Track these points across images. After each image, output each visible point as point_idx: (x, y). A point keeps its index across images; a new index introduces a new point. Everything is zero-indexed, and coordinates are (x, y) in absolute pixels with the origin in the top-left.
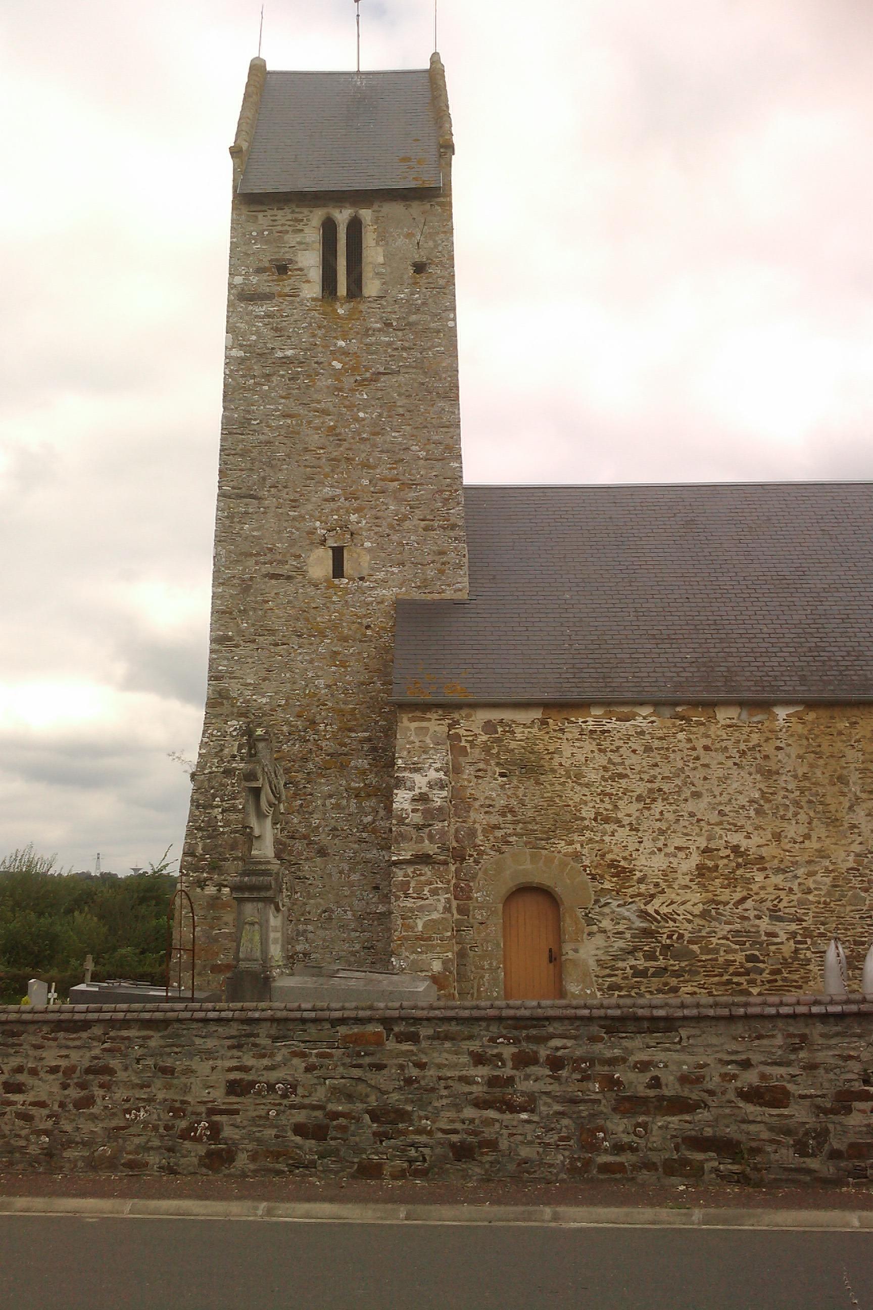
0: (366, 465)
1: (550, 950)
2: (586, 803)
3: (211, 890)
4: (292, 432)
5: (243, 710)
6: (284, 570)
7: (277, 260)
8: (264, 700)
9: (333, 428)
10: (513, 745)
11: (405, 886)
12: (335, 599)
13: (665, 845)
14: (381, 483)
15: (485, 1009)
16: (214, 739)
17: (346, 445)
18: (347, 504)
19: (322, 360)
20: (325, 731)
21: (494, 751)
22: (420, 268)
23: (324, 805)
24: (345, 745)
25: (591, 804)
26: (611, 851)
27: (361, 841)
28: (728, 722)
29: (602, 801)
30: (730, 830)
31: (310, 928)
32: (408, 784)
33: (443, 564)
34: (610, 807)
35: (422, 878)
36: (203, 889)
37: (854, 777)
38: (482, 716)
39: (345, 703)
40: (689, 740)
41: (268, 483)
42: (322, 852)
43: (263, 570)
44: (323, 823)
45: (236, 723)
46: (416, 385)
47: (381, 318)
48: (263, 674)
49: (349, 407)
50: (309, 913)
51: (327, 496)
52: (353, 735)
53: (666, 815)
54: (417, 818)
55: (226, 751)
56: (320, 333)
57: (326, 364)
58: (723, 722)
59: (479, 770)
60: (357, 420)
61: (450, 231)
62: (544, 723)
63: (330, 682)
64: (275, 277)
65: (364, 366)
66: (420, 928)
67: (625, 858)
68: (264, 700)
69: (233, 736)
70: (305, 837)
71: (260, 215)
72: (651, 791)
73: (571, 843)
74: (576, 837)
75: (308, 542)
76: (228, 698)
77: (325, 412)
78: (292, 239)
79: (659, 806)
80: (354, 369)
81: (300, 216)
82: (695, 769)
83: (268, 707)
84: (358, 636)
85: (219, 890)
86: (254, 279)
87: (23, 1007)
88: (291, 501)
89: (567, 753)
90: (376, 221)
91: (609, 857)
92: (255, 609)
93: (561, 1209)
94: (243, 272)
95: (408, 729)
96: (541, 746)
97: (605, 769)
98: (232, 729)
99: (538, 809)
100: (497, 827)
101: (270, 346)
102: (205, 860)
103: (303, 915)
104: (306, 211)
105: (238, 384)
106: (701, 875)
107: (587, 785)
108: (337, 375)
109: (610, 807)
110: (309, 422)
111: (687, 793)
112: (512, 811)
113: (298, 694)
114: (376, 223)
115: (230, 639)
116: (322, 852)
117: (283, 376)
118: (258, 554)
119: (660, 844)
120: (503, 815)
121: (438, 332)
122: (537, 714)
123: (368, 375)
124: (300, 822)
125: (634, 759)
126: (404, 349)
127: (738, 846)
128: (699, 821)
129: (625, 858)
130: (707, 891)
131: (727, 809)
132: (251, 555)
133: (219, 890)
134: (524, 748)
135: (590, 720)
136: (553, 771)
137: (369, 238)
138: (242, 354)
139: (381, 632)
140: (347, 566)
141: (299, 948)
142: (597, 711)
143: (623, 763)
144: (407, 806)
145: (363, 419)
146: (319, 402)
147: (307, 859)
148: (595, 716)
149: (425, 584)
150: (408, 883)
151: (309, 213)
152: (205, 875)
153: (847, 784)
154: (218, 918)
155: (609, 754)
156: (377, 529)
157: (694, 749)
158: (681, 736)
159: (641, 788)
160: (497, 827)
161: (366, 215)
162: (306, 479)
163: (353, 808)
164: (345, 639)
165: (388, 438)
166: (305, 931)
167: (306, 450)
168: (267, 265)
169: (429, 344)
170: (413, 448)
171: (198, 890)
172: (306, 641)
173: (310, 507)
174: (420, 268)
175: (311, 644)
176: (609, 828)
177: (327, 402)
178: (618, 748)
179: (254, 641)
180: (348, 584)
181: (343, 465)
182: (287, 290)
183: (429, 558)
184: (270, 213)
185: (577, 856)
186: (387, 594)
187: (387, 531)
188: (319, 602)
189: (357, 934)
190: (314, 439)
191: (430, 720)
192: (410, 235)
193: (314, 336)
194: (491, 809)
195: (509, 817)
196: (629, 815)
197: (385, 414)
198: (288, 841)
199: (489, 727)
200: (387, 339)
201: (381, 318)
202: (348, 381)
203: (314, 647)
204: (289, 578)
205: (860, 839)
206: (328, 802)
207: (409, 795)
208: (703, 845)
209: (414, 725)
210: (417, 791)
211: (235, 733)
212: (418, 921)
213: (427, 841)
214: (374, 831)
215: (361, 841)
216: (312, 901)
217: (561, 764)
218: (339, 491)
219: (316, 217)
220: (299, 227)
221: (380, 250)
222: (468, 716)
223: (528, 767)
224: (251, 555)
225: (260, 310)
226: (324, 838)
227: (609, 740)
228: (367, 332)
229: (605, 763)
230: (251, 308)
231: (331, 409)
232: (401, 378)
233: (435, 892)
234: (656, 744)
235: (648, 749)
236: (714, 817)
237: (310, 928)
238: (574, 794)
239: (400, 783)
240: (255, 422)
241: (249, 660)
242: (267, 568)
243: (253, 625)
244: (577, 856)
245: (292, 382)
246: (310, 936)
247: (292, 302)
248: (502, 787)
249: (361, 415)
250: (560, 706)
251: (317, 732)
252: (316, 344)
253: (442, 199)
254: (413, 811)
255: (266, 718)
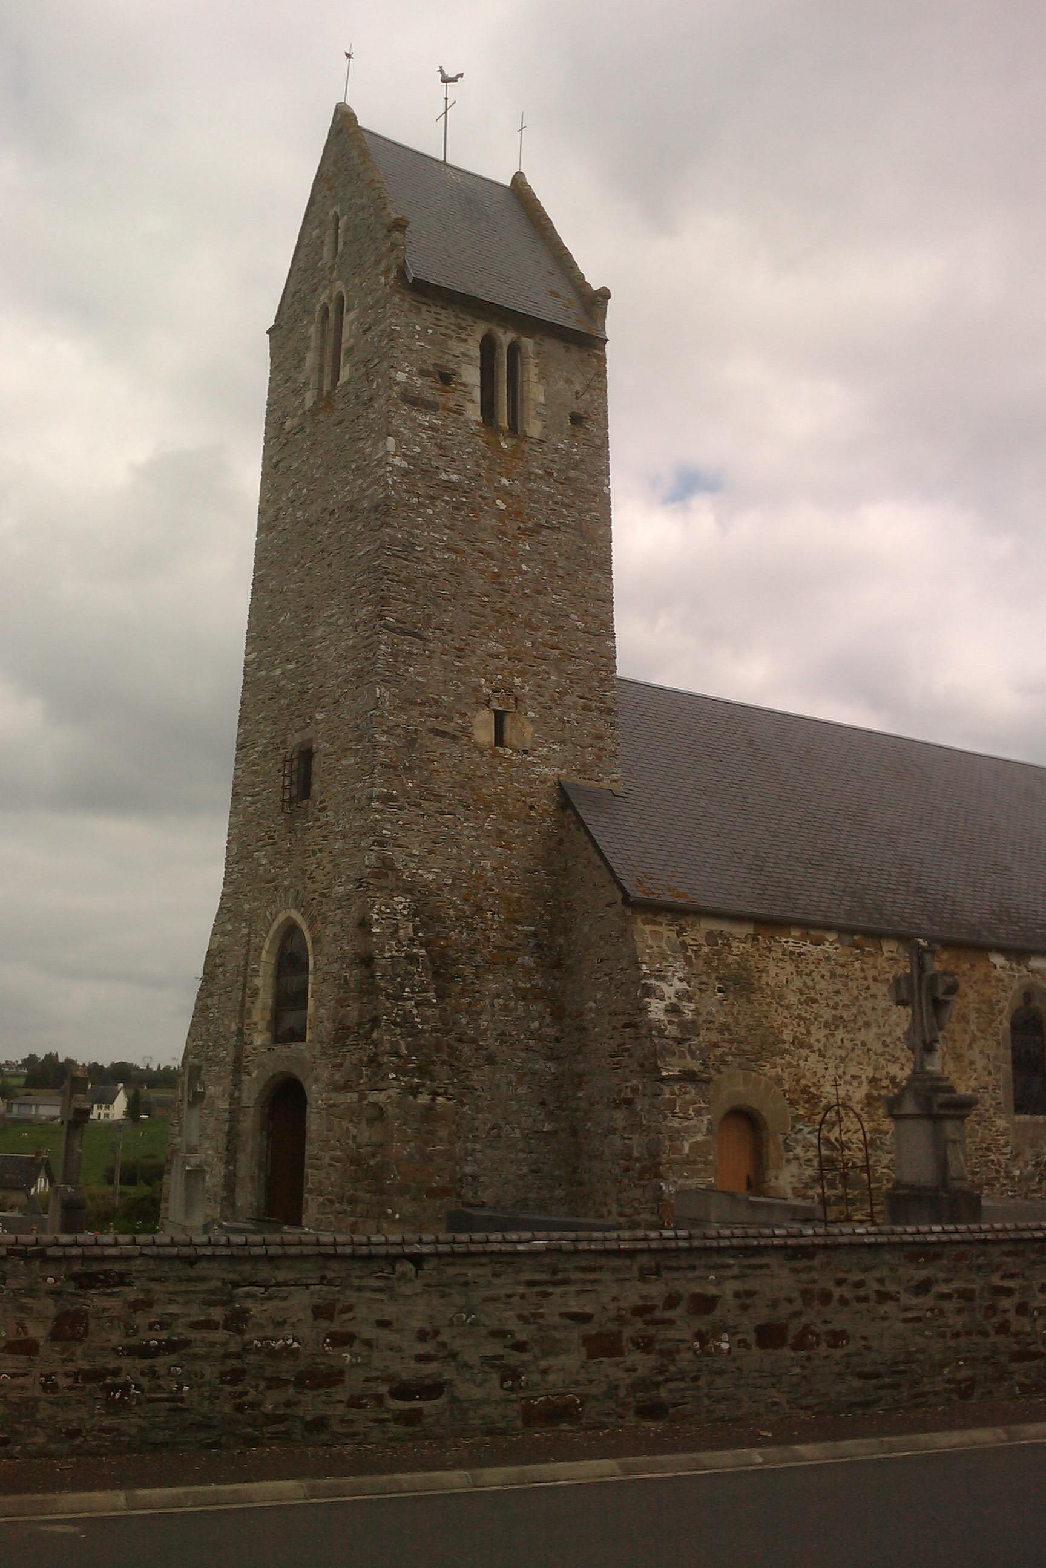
0: (528, 625)
1: (748, 1177)
2: (786, 1026)
3: (424, 1099)
4: (457, 570)
5: (409, 885)
6: (450, 727)
7: (440, 366)
8: (431, 877)
9: (496, 576)
10: (731, 959)
11: (672, 1104)
12: (500, 769)
13: (844, 1073)
14: (542, 649)
15: (412, 1244)
16: (384, 916)
17: (509, 597)
18: (510, 665)
19: (487, 495)
20: (493, 920)
21: (715, 964)
22: (576, 419)
23: (492, 1005)
24: (511, 938)
25: (790, 1027)
26: (804, 1077)
27: (528, 1049)
28: (890, 954)
29: (799, 1025)
30: (889, 1061)
31: (478, 1147)
32: (658, 993)
33: (600, 749)
34: (804, 1031)
35: (687, 1097)
36: (415, 1097)
37: (973, 1016)
38: (707, 925)
39: (512, 891)
40: (863, 970)
41: (434, 623)
42: (491, 1060)
43: (428, 723)
44: (492, 1026)
45: (403, 900)
46: (575, 547)
47: (543, 464)
48: (428, 845)
49: (513, 555)
50: (477, 1129)
51: (491, 651)
52: (520, 928)
53: (846, 1042)
54: (672, 1031)
55: (401, 933)
56: (485, 463)
57: (490, 501)
58: (886, 955)
59: (703, 983)
60: (521, 572)
61: (604, 389)
62: (755, 939)
63: (496, 865)
64: (438, 386)
65: (527, 514)
66: (686, 1150)
67: (814, 1085)
68: (431, 877)
69: (404, 916)
70: (473, 1041)
71: (424, 308)
72: (834, 1016)
73: (774, 1066)
74: (778, 1061)
75: (474, 700)
76: (393, 869)
77: (489, 555)
78: (457, 348)
79: (840, 1034)
80: (518, 514)
81: (464, 324)
82: (866, 998)
83: (433, 886)
84: (523, 816)
85: (433, 1100)
86: (418, 381)
87: (160, 1238)
88: (457, 649)
89: (772, 974)
90: (538, 354)
91: (803, 1082)
92: (420, 768)
93: (1014, 1428)
94: (407, 370)
95: (643, 931)
96: (752, 963)
97: (801, 993)
98: (401, 907)
99: (749, 1028)
100: (716, 1045)
101: (434, 464)
102: (412, 1062)
103: (471, 1131)
104: (470, 320)
105: (402, 498)
106: (869, 1104)
107: (788, 1007)
108: (501, 515)
109: (804, 1031)
110: (474, 563)
111: (860, 1022)
112: (729, 1030)
113: (464, 874)
114: (538, 358)
115: (394, 799)
116: (491, 1060)
117: (446, 502)
118: (422, 704)
119: (840, 1072)
120: (721, 1032)
121: (595, 495)
122: (749, 929)
123: (530, 524)
124: (468, 1023)
125: (822, 985)
126: (564, 505)
127: (895, 1077)
128: (869, 1050)
129: (814, 1085)
130: (873, 1121)
131: (888, 1040)
132: (416, 703)
133: (433, 1100)
134: (738, 963)
135: (790, 941)
136: (761, 990)
137: (531, 371)
138: (404, 464)
139: (545, 815)
140: (509, 734)
141: (468, 1169)
142: (796, 933)
143: (814, 988)
144: (662, 1016)
145: (526, 573)
146: (483, 542)
147: (475, 1066)
148: (795, 938)
149: (584, 769)
150: (674, 1100)
151: (471, 323)
152: (416, 1080)
153: (968, 1022)
154: (432, 1133)
155: (804, 977)
156: (540, 699)
157: (865, 978)
158: (857, 964)
159: (827, 1014)
160: (716, 1045)
161: (528, 344)
162: (472, 627)
163: (520, 1012)
164: (509, 817)
165: (549, 600)
166: (474, 1150)
167: (471, 594)
168: (431, 369)
169: (587, 506)
170: (573, 616)
171: (411, 1098)
172: (472, 814)
173: (475, 660)
174: (576, 419)
175: (477, 818)
176: (805, 1052)
177: (491, 545)
178: (812, 971)
179: (419, 805)
180: (512, 754)
181: (507, 620)
182: (451, 404)
183: (588, 741)
184: (433, 309)
185: (779, 1080)
186: (549, 772)
187: (550, 703)
188: (484, 770)
189: (525, 1156)
190: (479, 583)
191: (660, 924)
192: (568, 381)
193: (478, 465)
194: (711, 1025)
195: (727, 1036)
196: (818, 1041)
197: (547, 572)
198: (456, 1044)
199: (711, 937)
200: (548, 489)
201: (543, 464)
202: (512, 526)
203: (480, 822)
204: (454, 738)
205: (975, 1075)
206: (496, 1002)
207: (661, 1005)
208: (871, 1075)
209: (648, 928)
210: (668, 1002)
211: (405, 912)
212: (685, 1143)
213: (688, 1057)
214: (540, 1039)
215: (528, 1049)
216: (480, 1116)
217: (768, 984)
218: (503, 649)
219: (480, 330)
220: (463, 336)
221: (541, 388)
222: (693, 925)
223: (740, 984)
224: (416, 703)
225: (425, 419)
226: (491, 1043)
227: (804, 962)
228: (529, 477)
229: (801, 986)
230: (414, 413)
231: (496, 553)
232: (560, 536)
233: (699, 1112)
234: (839, 971)
235: (833, 975)
236: (879, 1048)
237: (478, 1147)
238: (778, 1017)
239: (649, 991)
240: (419, 549)
241: (414, 827)
242: (432, 722)
243: (419, 786)
244: (779, 1080)
245: (456, 512)
246: (479, 1156)
247: (455, 420)
248: (721, 1002)
249: (524, 567)
250: (768, 925)
251: (484, 920)
252: (480, 476)
253: (596, 351)
254: (670, 1023)
255: (432, 898)
